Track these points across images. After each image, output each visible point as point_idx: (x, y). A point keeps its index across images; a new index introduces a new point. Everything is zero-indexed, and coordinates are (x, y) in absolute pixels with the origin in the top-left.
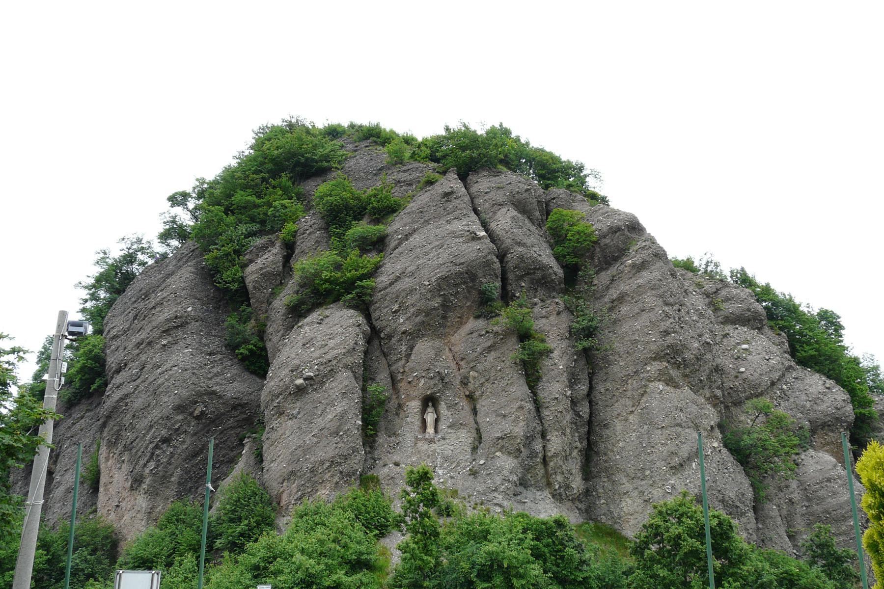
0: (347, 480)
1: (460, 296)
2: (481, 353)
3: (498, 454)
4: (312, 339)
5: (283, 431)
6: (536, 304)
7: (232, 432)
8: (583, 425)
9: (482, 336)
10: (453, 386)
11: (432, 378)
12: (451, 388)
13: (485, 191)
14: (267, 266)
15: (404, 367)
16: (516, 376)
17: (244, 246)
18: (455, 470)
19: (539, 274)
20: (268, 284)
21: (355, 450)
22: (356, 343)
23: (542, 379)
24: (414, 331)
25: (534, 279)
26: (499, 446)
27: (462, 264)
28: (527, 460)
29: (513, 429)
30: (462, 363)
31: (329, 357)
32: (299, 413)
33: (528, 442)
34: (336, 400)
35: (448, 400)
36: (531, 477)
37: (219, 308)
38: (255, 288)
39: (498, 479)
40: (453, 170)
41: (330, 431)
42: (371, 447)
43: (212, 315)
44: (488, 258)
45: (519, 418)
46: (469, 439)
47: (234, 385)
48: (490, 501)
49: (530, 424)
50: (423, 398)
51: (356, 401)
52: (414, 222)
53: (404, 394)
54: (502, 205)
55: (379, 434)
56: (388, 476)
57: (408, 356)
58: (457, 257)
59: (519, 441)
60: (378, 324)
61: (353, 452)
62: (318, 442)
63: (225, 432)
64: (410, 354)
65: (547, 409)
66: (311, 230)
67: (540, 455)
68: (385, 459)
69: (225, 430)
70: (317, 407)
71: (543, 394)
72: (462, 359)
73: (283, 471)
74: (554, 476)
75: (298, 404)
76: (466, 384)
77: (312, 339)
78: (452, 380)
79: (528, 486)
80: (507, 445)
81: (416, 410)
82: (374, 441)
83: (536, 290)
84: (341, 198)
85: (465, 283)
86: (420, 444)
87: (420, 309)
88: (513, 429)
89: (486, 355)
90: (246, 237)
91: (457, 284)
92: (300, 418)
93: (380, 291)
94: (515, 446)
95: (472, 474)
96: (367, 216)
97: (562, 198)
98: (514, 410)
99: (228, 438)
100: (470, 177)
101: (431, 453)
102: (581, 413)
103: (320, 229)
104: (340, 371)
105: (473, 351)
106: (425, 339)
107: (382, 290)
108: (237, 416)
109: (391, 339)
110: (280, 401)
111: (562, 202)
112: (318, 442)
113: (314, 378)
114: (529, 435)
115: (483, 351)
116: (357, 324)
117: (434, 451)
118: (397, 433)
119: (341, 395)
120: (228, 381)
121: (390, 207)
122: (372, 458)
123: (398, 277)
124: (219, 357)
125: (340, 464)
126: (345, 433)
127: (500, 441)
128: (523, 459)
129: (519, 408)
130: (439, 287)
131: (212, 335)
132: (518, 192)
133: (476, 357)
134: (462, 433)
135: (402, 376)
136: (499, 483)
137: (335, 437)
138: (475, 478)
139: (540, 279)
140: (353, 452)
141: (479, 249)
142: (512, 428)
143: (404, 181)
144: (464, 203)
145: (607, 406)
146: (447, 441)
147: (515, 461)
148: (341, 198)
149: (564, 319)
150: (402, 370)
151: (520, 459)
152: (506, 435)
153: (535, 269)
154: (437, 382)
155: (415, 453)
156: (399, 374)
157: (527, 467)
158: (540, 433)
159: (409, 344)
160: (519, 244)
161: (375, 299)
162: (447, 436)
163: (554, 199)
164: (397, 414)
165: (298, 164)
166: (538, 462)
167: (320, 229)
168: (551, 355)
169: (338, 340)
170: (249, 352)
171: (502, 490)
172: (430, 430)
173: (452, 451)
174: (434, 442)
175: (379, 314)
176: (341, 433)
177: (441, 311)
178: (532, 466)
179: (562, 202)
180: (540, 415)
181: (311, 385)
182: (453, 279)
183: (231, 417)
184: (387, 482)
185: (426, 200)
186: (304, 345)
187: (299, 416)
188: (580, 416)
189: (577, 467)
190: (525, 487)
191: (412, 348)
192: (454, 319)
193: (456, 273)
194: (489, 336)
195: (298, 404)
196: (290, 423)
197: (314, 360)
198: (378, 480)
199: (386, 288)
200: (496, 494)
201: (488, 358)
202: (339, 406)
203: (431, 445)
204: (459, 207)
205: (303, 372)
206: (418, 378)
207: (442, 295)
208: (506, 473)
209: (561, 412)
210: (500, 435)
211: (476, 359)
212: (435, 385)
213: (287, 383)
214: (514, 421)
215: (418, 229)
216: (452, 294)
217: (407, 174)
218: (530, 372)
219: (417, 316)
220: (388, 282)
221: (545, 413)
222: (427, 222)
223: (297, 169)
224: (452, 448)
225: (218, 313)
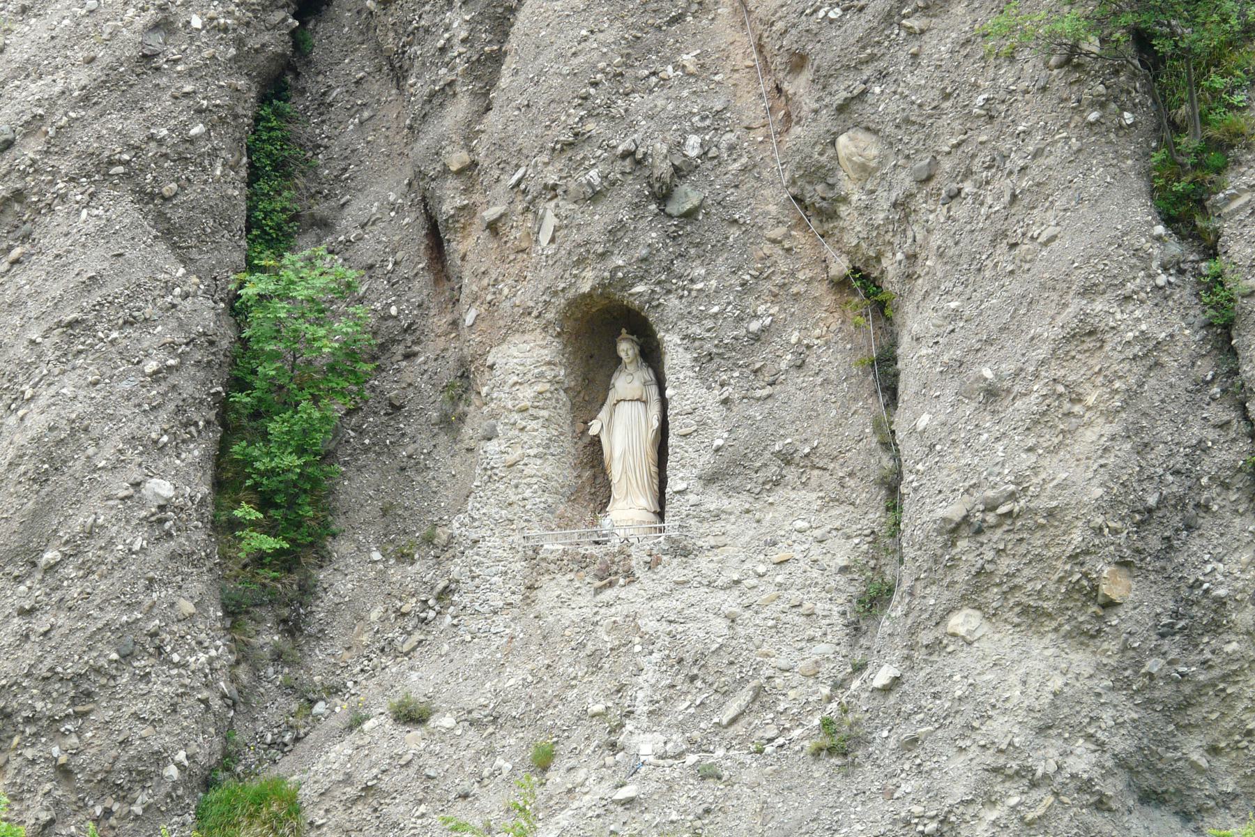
10: (734, 233)
11: (595, 196)
12: (721, 246)
15: (469, 136)
16: (1066, 142)
18: (739, 728)
26: (961, 577)
28: (1156, 651)
29: (1035, 469)
33: (1155, 543)
35: (701, 317)
36: (1214, 750)
42: (291, 628)
45: (1078, 400)
46: (835, 543)
49: (1164, 430)
50: (572, 304)
55: (341, 547)
56: (348, 780)
59: (1077, 537)
61: (127, 657)
64: (497, 59)
72: (798, 62)
78: (733, 195)
80: (1006, 565)
81: (526, 394)
82: (307, 591)
86: (551, 590)
89: (915, 23)
94: (1063, 567)
95: (831, 751)
98: (1043, 352)
101: (610, 641)
104: (63, 198)
114: (1152, 500)
118: (442, 535)
119: (55, 337)
122: (290, 688)
127: (962, 544)
128: (1125, 648)
133: (863, 43)
136: (959, 792)
137: (18, 580)
138: (849, 769)
146: (703, 563)
147: (1081, 660)
150: (457, 159)
152: (991, 507)
154: (624, 215)
157: (1164, 691)
164: (450, 423)
166: (1230, 659)
176: (51, 555)
178: (1200, 689)
180: (1235, 372)
184: (339, 815)
201: (929, 42)
202: (42, 402)
203: (608, 595)
208: (1000, 728)
210: (955, 511)
212: (615, 233)
214: (1038, 421)
224: (730, 601)
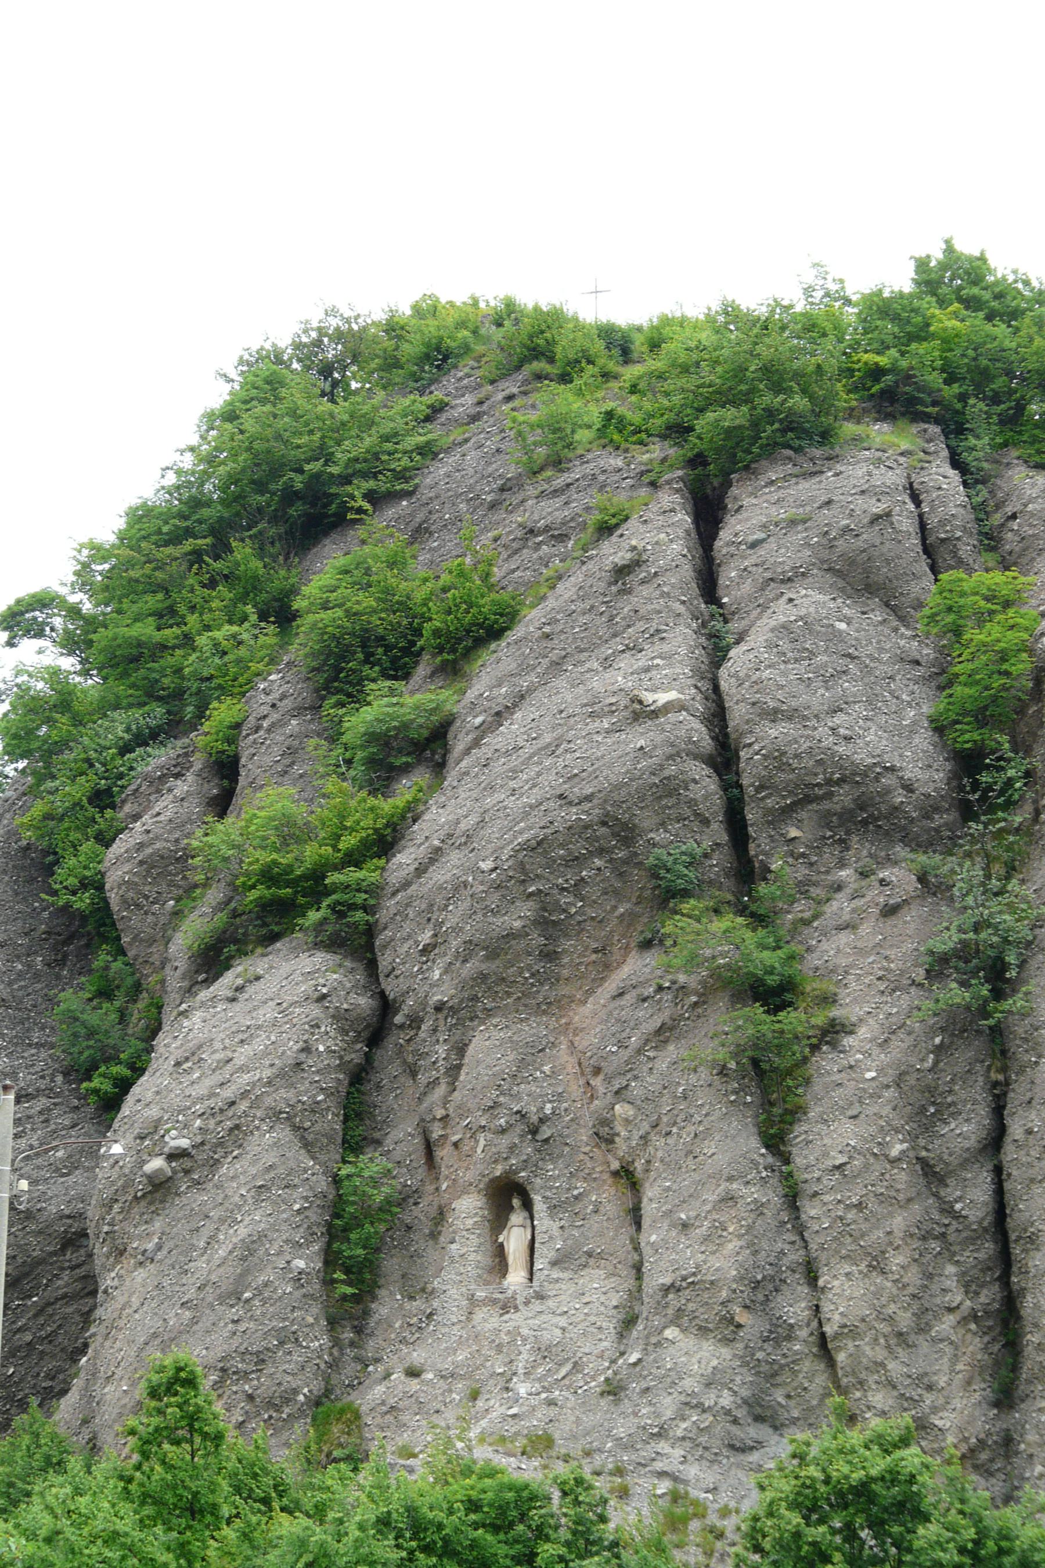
0: (271, 1417)
1: (592, 892)
2: (639, 1051)
3: (670, 1333)
4: (200, 1047)
5: (125, 1299)
6: (839, 888)
7: (69, 1310)
8: (972, 1240)
9: (644, 1000)
10: (567, 1149)
11: (503, 1131)
12: (561, 1155)
13: (752, 538)
14: (157, 838)
15: (445, 1102)
17: (121, 776)
18: (566, 1382)
19: (844, 797)
20: (164, 887)
21: (287, 1338)
22: (306, 1049)
23: (805, 1113)
24: (461, 1001)
25: (829, 813)
26: (670, 1311)
27: (588, 798)
28: (761, 1349)
29: (705, 1262)
30: (597, 1082)
31: (228, 1093)
32: (159, 1247)
33: (760, 1297)
34: (239, 1207)
35: (551, 1188)
36: (788, 1397)
37: (62, 962)
38: (125, 902)
39: (668, 1404)
40: (669, 482)
41: (218, 1291)
42: (359, 1330)
43: (38, 986)
44: (666, 773)
45: (725, 1230)
47: (71, 1179)
48: (644, 1466)
51: (297, 1207)
52: (524, 669)
53: (447, 1177)
54: (789, 580)
56: (383, 1403)
57: (454, 1071)
58: (576, 780)
59: (724, 1294)
60: (391, 988)
61: (282, 1343)
62: (194, 1321)
63: (50, 1310)
64: (459, 1067)
65: (816, 1201)
66: (275, 716)
67: (803, 1333)
68: (391, 1360)
69: (49, 1304)
70: (197, 1230)
71: (805, 1158)
72: (597, 1070)
73: (123, 1402)
74: (858, 1394)
75: (158, 1225)
76: (610, 1141)
77: (200, 1047)
78: (566, 1132)
79: (782, 1425)
80: (691, 1306)
81: (470, 1222)
82: (366, 1313)
83: (843, 844)
84: (349, 613)
85: (601, 852)
86: (479, 1315)
87: (470, 941)
88: (705, 1262)
89: (651, 1054)
90: (125, 749)
91: (577, 858)
92: (161, 1261)
93: (394, 894)
95: (609, 1393)
96: (426, 657)
97: (1032, 515)
99: (60, 1327)
100: (734, 491)
101: (506, 1339)
102: (958, 1206)
103: (298, 711)
104: (258, 1128)
105: (622, 1045)
106: (495, 1021)
107: (398, 891)
108: (78, 1266)
109: (419, 1028)
110: (113, 1218)
111: (1031, 525)
112: (194, 1321)
113: (194, 1152)
114: (759, 1277)
115: (645, 1044)
116: (316, 995)
117: (515, 1333)
118: (429, 1287)
120: (57, 1170)
121: (481, 626)
122: (357, 1359)
123: (438, 850)
124: (43, 1102)
125: (245, 1375)
126: (259, 1292)
127: (671, 1296)
128: (747, 1347)
129: (723, 1200)
130: (523, 874)
131: (30, 1045)
132: (846, 530)
134: (591, 1281)
135: (444, 1128)
136: (669, 1414)
137: (232, 1306)
138: (617, 1402)
139: (851, 811)
140: (282, 1343)
141: (642, 748)
142: (701, 1257)
143: (547, 529)
144: (663, 595)
145: (1032, 1180)
146: (551, 1303)
148: (349, 613)
149: (913, 926)
151: (740, 1346)
152: (684, 1279)
153: (829, 782)
155: (467, 1340)
156: (437, 1124)
158: (801, 1269)
159: (453, 1039)
160: (774, 715)
161: (383, 916)
162: (550, 1290)
163: (1014, 517)
164: (434, 1236)
165: (290, 496)
166: (796, 1353)
167: (298, 711)
168: (845, 1042)
169: (259, 1045)
170: (115, 1086)
171: (680, 1433)
172: (516, 1277)
173: (563, 1329)
174: (516, 1308)
175: (390, 959)
176: (247, 1295)
177: (537, 939)
178: (782, 1367)
179: (1031, 525)
180: (798, 1218)
181: (187, 1172)
182: (561, 846)
183: (63, 1269)
184: (379, 1420)
185: (566, 596)
186: (178, 1064)
187: (159, 1256)
188: (957, 1216)
189: (960, 1367)
190: (775, 1428)
191: (461, 1049)
192: (581, 955)
193: (570, 827)
194: (661, 999)
195: (157, 1225)
196: (140, 1274)
197: (194, 1104)
198: (358, 1416)
199: (406, 884)
200: (663, 1446)
202: (246, 1223)
203: (506, 1317)
204: (642, 612)
205: (167, 1138)
206: (474, 1132)
207: (531, 894)
208: (689, 1384)
209: (859, 1206)
210: (667, 1280)
211: (629, 1069)
212: (512, 1148)
213: (127, 1171)
214: (706, 1239)
215: (531, 690)
216: (564, 889)
217: (559, 501)
218: (775, 1096)
219: (465, 961)
220: (412, 868)
221: (811, 1210)
222: (557, 665)
223: (292, 511)
224: (563, 1321)
225: (58, 977)
